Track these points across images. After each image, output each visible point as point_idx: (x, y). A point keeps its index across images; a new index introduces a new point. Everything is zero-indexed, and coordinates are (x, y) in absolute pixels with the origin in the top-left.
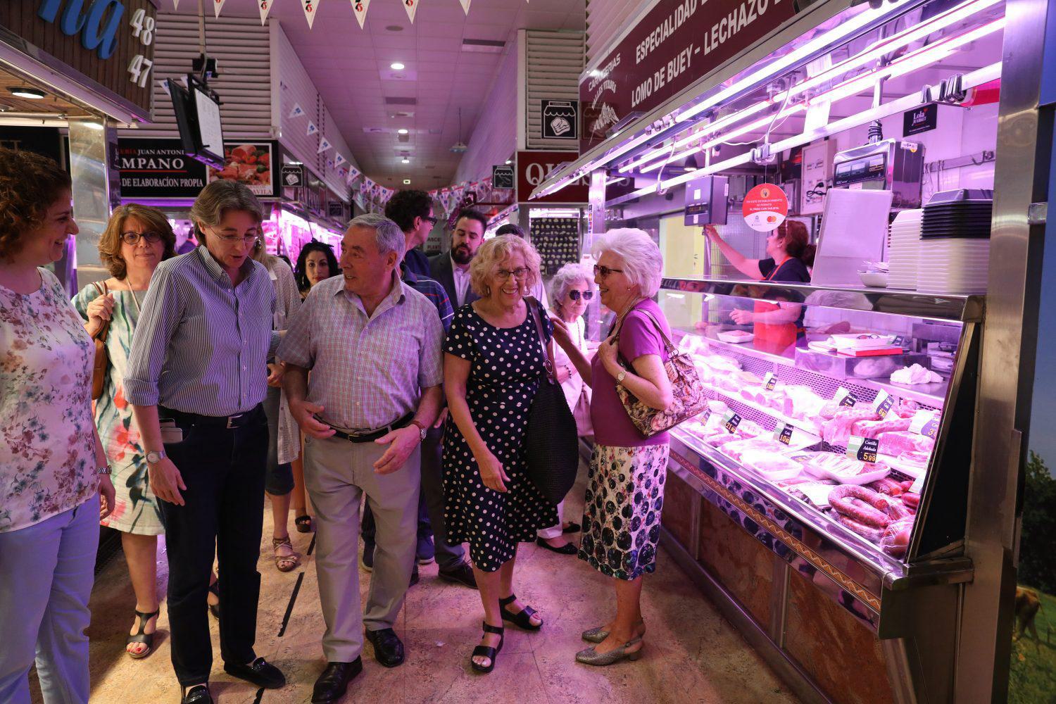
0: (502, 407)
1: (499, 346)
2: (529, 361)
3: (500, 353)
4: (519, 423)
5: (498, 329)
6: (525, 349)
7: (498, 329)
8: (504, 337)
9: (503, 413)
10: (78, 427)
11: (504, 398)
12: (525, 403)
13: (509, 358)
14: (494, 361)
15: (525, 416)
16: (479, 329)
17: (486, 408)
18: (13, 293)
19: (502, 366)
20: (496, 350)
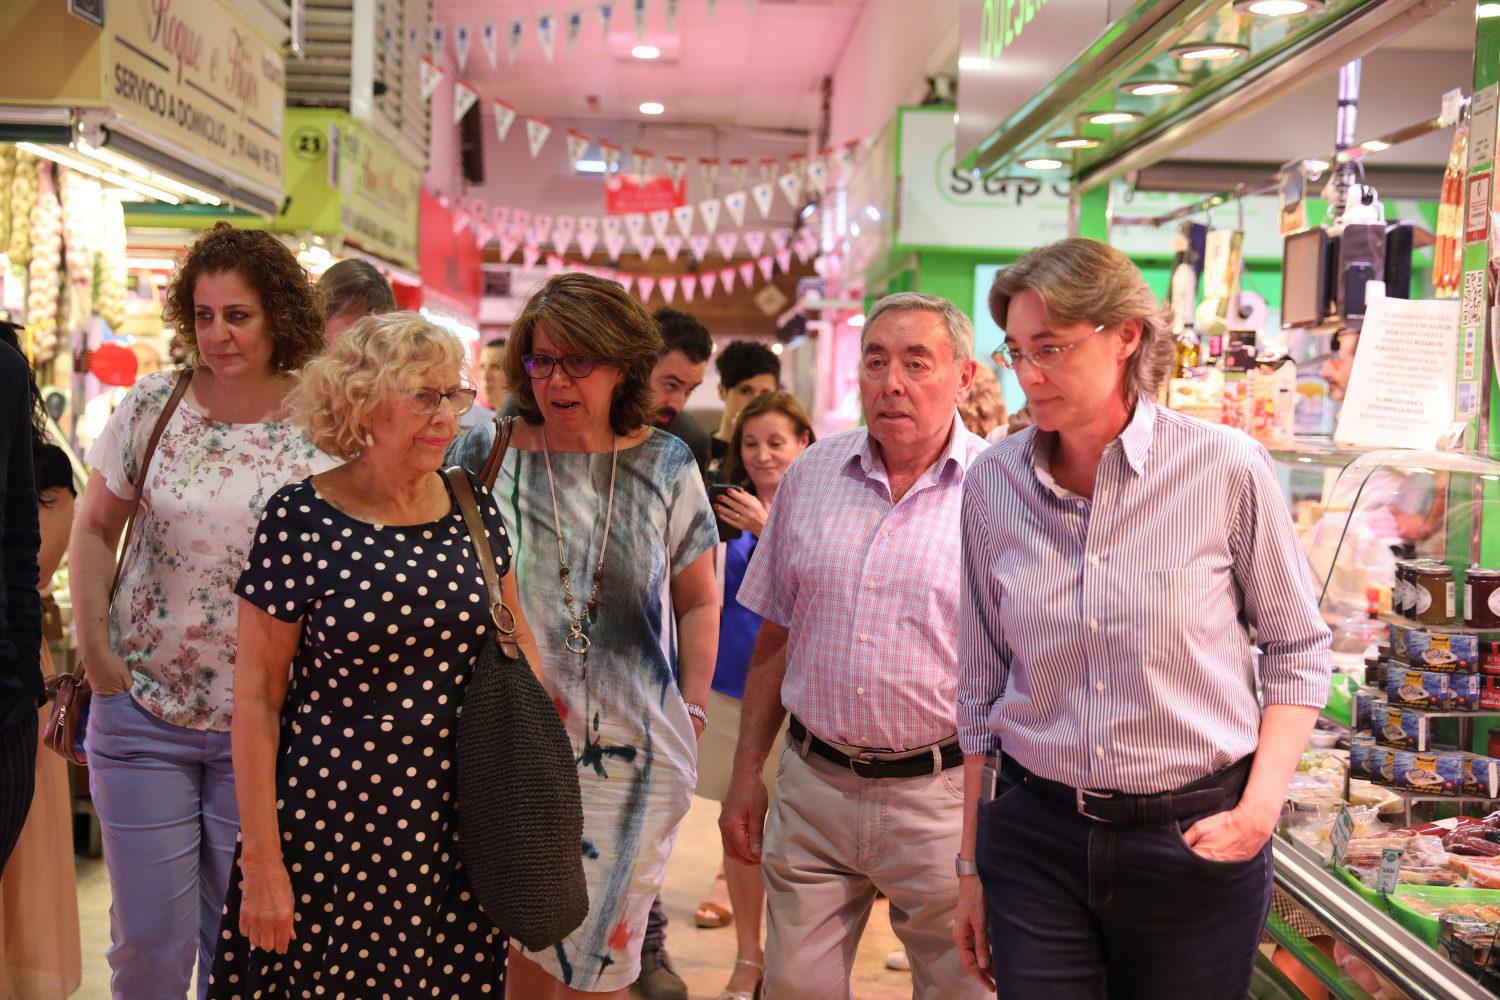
0: (387, 727)
1: (380, 566)
2: (458, 601)
3: (383, 582)
4: (428, 768)
5: (378, 527)
6: (447, 573)
7: (378, 527)
8: (395, 545)
9: (389, 743)
10: (211, 620)
11: (392, 703)
12: (444, 717)
13: (405, 594)
14: (369, 601)
15: (444, 749)
16: (329, 535)
17: (349, 732)
18: (198, 414)
19: (388, 613)
20: (373, 576)
